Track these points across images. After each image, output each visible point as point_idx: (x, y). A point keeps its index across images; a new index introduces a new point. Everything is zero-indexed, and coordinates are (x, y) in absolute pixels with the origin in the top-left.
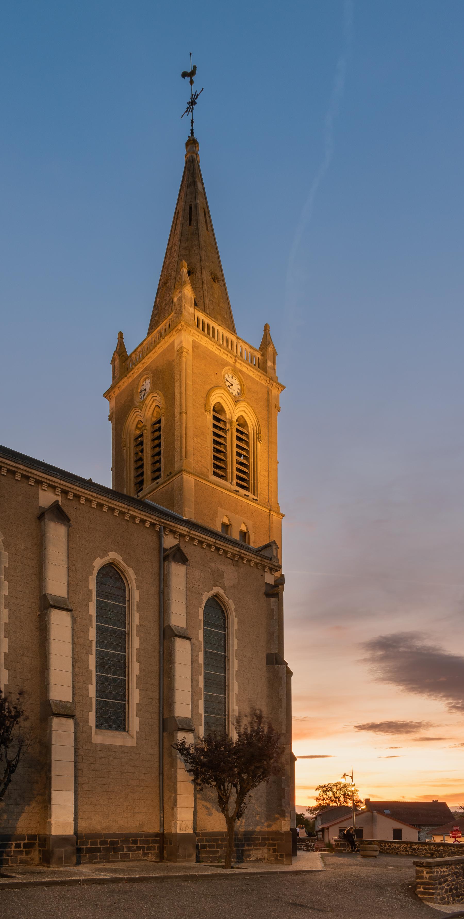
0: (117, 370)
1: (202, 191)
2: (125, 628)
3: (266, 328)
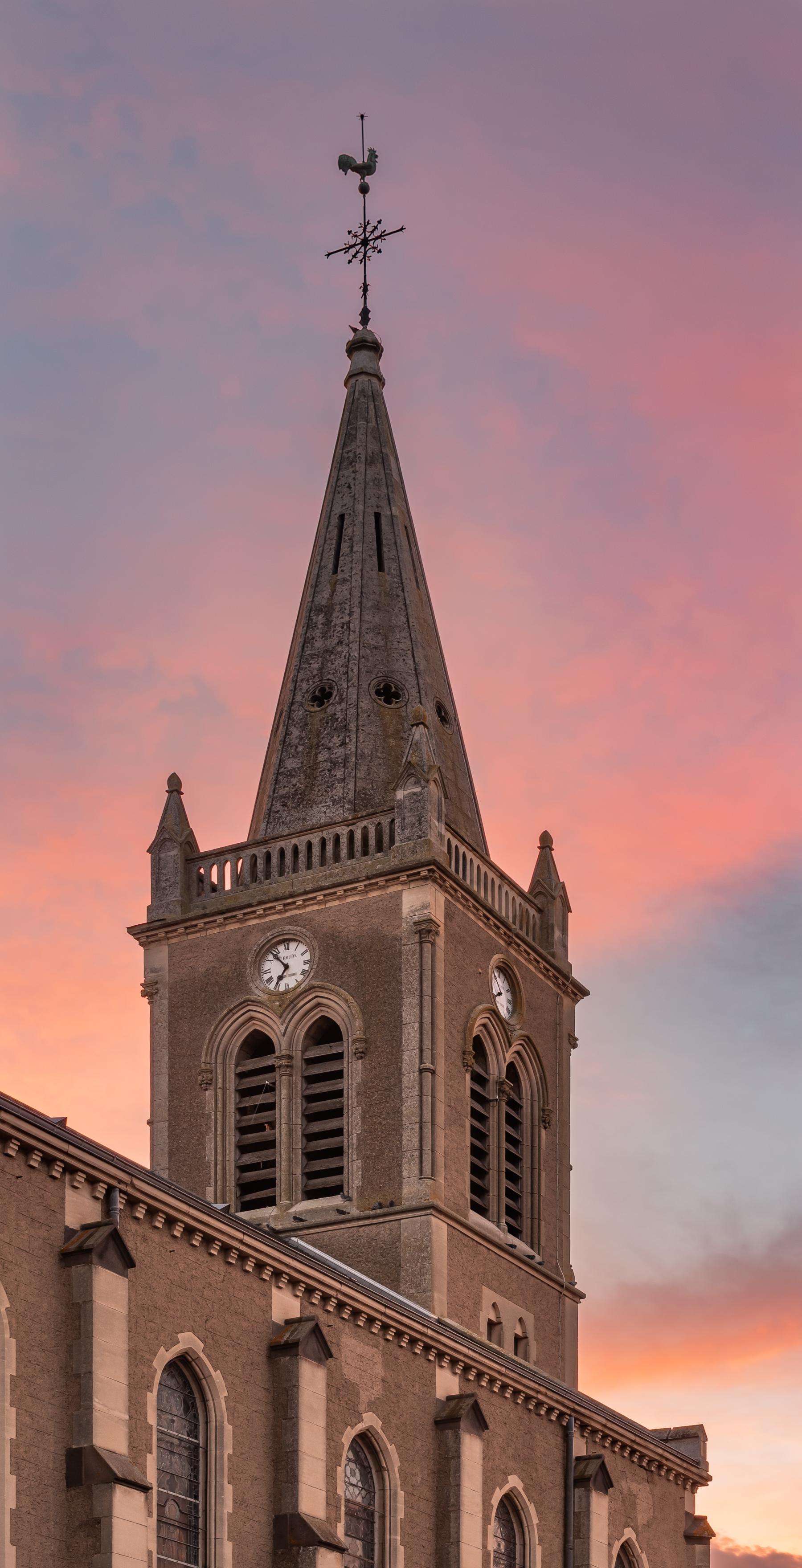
1: (398, 480)
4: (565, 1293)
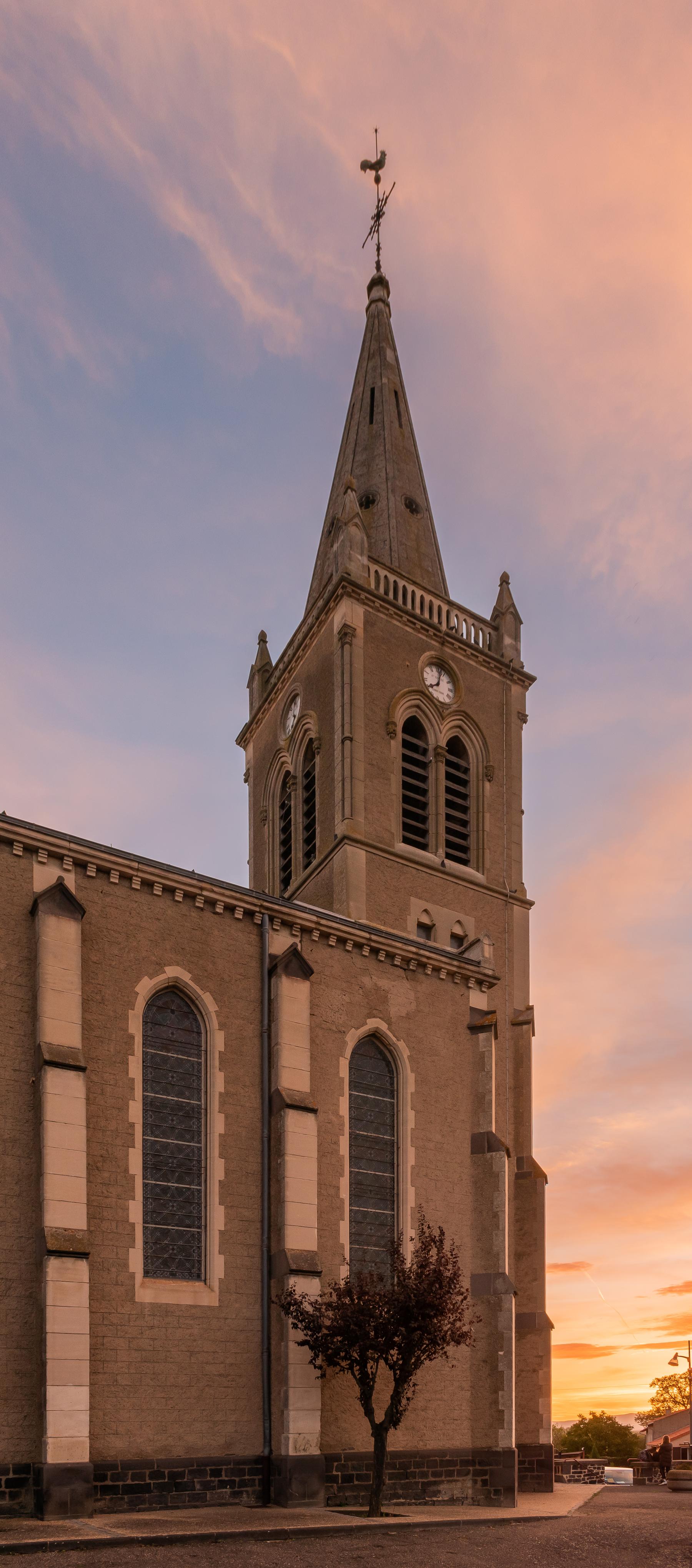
0: (256, 695)
1: (393, 362)
2: (199, 1100)
3: (505, 580)
4: (511, 901)
